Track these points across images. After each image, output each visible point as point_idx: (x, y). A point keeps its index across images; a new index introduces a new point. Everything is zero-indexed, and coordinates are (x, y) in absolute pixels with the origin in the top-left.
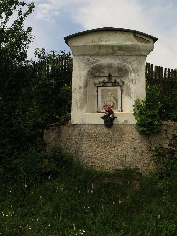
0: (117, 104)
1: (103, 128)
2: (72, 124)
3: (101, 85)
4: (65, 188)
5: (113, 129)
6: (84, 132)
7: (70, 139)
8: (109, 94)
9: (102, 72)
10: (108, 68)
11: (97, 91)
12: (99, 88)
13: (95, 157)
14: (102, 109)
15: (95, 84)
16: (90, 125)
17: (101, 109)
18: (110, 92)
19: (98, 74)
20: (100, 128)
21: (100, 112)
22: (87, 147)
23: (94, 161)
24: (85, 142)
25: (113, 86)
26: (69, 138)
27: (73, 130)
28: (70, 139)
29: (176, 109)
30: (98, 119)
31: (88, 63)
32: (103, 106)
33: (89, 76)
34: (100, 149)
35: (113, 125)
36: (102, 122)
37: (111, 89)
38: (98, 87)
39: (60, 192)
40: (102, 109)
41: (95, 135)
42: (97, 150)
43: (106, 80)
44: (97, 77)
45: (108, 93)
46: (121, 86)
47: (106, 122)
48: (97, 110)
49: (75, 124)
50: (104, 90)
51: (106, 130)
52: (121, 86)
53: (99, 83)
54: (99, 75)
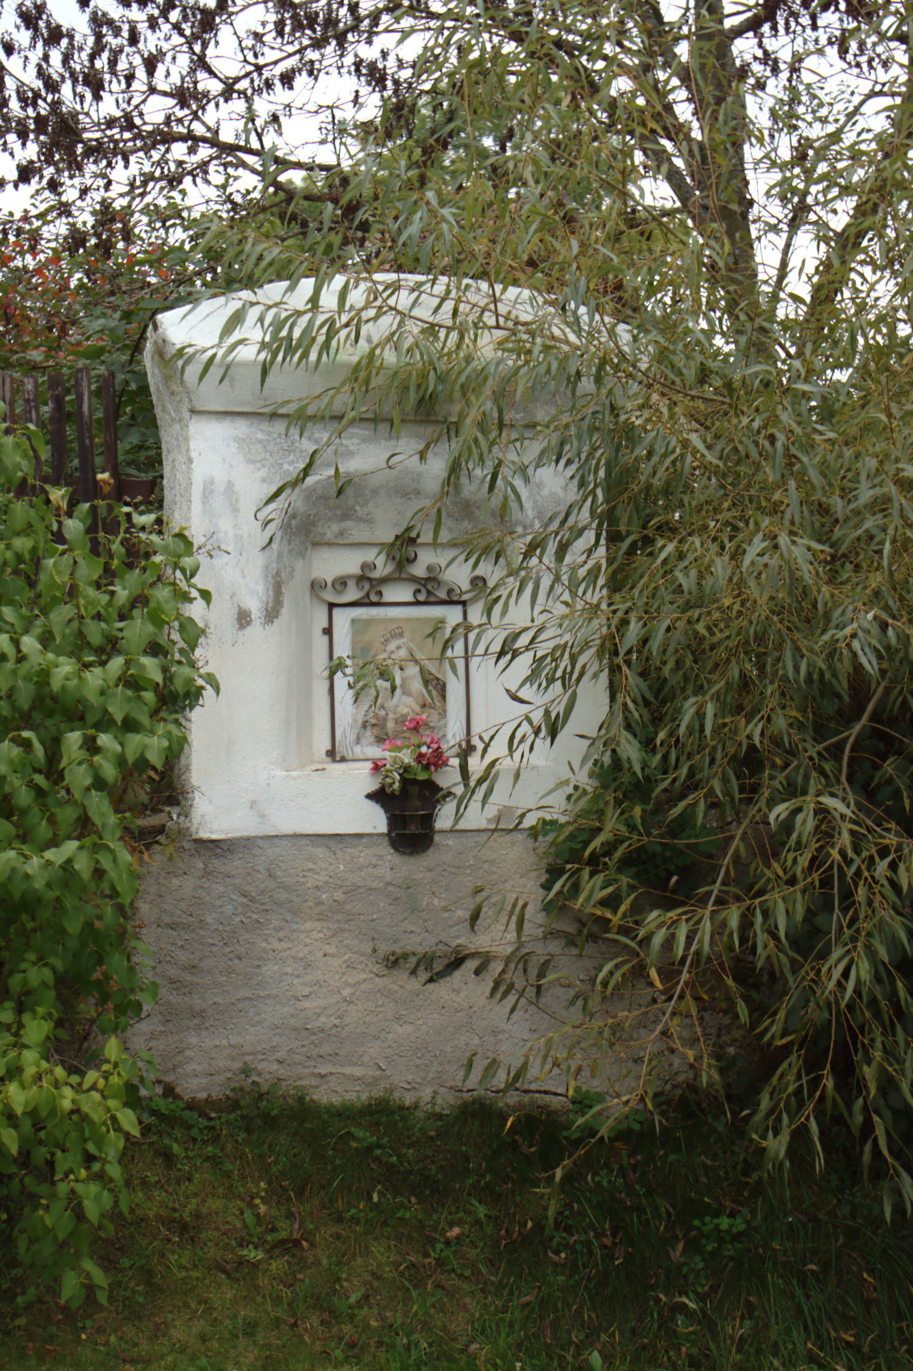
0: (443, 714)
1: (381, 857)
2: (196, 841)
3: (353, 593)
4: (99, 1228)
5: (430, 858)
6: (272, 885)
7: (187, 927)
8: (398, 648)
9: (360, 520)
10: (399, 500)
11: (328, 631)
12: (336, 612)
13: (337, 1022)
14: (358, 741)
15: (316, 587)
16: (304, 841)
17: (351, 737)
18: (401, 635)
19: (335, 528)
20: (364, 855)
21: (343, 760)
22: (289, 970)
23: (325, 1049)
24: (280, 940)
25: (418, 603)
26: (186, 919)
27: (207, 874)
28: (187, 927)
29: (909, 407)
30: (345, 803)
31: (286, 466)
32: (360, 722)
33: (289, 542)
34: (363, 976)
35: (437, 838)
36: (376, 820)
37: (408, 620)
38: (332, 606)
39: (556, 1064)
40: (358, 741)
41: (339, 895)
42: (348, 985)
43: (383, 568)
44: (329, 544)
45: (392, 646)
46: (464, 603)
47: (394, 821)
48: (329, 747)
49: (214, 837)
50: (369, 622)
51: (390, 864)
52: (464, 603)
53: (341, 583)
54: (341, 533)
